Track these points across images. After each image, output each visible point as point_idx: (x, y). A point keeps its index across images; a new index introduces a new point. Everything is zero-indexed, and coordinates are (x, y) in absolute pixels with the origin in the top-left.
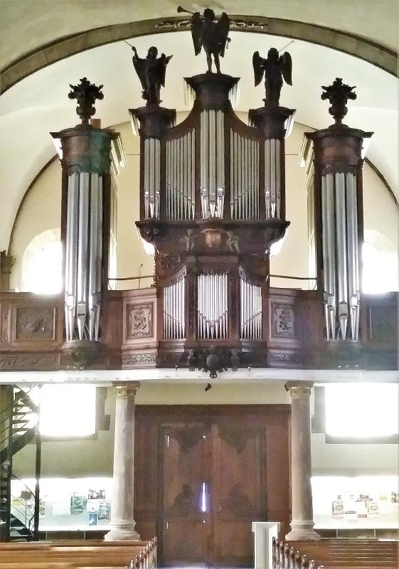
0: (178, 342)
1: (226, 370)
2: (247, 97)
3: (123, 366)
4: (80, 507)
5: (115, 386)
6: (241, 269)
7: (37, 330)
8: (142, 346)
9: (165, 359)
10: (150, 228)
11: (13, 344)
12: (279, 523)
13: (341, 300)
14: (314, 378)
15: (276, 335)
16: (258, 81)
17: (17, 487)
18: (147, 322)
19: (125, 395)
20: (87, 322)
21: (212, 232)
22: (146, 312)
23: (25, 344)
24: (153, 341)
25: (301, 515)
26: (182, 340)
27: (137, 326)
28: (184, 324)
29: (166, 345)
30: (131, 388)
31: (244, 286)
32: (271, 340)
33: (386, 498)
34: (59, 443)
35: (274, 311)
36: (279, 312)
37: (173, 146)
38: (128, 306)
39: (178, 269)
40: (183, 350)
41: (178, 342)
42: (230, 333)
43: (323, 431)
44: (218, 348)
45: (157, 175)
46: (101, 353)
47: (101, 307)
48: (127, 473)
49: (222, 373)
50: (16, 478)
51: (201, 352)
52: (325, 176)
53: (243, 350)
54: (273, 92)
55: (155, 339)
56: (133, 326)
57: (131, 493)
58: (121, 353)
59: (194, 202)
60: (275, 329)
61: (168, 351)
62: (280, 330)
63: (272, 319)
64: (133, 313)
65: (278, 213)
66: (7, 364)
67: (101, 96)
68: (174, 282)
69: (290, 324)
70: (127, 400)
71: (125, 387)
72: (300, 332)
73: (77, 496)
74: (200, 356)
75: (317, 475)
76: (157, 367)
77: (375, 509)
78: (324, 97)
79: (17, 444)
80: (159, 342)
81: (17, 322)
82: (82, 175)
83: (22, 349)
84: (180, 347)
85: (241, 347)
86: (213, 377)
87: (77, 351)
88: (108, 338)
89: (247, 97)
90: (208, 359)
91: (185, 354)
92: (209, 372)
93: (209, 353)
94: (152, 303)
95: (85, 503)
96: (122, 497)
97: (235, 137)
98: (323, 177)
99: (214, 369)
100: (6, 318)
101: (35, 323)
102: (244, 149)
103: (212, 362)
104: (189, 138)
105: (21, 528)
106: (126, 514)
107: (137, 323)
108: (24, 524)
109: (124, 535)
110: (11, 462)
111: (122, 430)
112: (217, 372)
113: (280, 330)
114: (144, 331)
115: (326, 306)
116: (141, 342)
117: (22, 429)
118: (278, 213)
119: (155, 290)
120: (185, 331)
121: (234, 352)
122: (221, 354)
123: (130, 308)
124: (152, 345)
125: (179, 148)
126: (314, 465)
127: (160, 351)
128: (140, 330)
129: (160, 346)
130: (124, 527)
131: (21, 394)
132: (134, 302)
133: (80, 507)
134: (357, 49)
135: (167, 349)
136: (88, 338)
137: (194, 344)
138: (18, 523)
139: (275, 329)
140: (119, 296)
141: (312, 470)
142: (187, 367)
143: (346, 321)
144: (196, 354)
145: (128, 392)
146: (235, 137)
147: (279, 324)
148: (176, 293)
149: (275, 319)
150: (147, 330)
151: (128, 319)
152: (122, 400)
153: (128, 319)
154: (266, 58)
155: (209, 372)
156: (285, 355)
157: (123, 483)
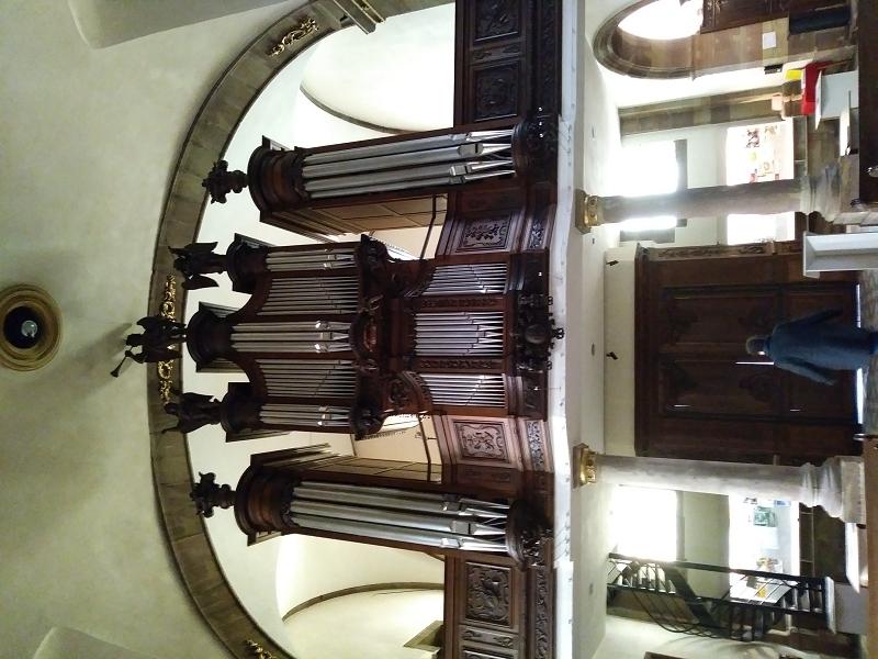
1: (551, 314)
2: (224, 294)
3: (548, 470)
4: (768, 515)
6: (410, 294)
7: (495, 593)
8: (515, 439)
9: (534, 406)
10: (364, 422)
12: (805, 234)
13: (457, 156)
14: (569, 188)
16: (213, 284)
17: (740, 590)
18: (482, 431)
21: (369, 337)
22: (469, 431)
23: (517, 618)
25: (792, 195)
26: (504, 379)
27: (489, 446)
28: (482, 377)
29: (513, 405)
30: (583, 458)
33: (755, 154)
34: (686, 545)
36: (471, 241)
37: (275, 387)
38: (464, 457)
39: (406, 383)
40: (519, 379)
44: (517, 327)
45: (303, 406)
46: (526, 505)
48: (718, 473)
49: (558, 321)
51: (522, 350)
52: (310, 193)
53: (520, 287)
54: (218, 264)
56: (490, 451)
57: (755, 469)
58: (528, 471)
59: (336, 362)
60: (496, 246)
62: (496, 239)
64: (472, 450)
66: (546, 645)
68: (426, 389)
69: (491, 225)
70: (603, 468)
71: (582, 467)
72: (502, 212)
73: (752, 518)
74: (528, 352)
76: (545, 419)
77: (768, 164)
78: (223, 200)
79: (685, 591)
82: (293, 509)
84: (515, 384)
85: (515, 291)
86: (562, 334)
89: (224, 294)
90: (532, 340)
91: (524, 374)
92: (555, 340)
93: (522, 340)
94: (455, 422)
95: (762, 509)
96: (763, 483)
97: (267, 310)
99: (550, 332)
100: (479, 636)
102: (283, 296)
103: (536, 334)
104: (267, 366)
105: (796, 592)
106: (796, 480)
107: (484, 445)
108: (789, 588)
109: (832, 484)
110: (709, 599)
111: (650, 478)
113: (496, 239)
114: (496, 436)
116: (510, 440)
119: (437, 417)
120: (487, 374)
122: (526, 320)
123: (465, 455)
124: (513, 426)
125: (279, 379)
128: (494, 440)
129: (514, 413)
130: (817, 485)
131: (625, 574)
132: (457, 450)
133: (768, 515)
134: (198, 175)
135: (518, 402)
136: (504, 519)
137: (509, 363)
138: (788, 596)
139: (496, 246)
140: (449, 466)
143: (484, 145)
144: (525, 360)
145: (590, 463)
146: (267, 310)
147: (488, 240)
150: (493, 431)
152: (602, 475)
155: (555, 340)
157: (739, 481)
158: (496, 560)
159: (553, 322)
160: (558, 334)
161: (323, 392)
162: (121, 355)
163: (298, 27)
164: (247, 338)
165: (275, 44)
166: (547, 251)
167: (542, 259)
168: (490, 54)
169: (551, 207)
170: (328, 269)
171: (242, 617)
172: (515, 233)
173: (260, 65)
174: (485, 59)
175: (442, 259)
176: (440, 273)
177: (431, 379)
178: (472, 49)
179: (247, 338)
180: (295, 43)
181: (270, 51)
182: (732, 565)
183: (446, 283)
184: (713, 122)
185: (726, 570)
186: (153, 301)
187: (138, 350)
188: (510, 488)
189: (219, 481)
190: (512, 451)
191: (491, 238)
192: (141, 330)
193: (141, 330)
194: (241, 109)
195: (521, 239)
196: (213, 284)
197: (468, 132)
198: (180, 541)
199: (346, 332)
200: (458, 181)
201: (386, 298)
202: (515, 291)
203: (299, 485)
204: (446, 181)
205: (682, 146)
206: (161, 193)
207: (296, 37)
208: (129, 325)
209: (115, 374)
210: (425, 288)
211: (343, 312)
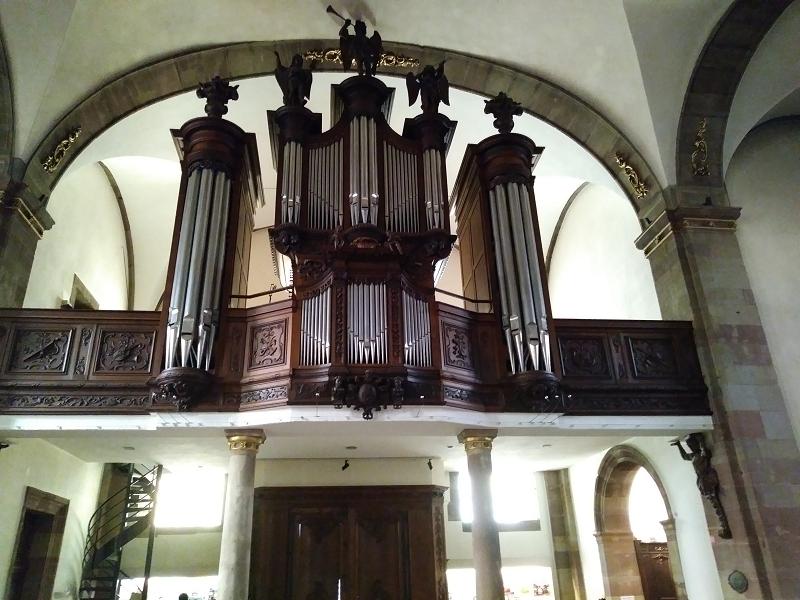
0: (321, 369)
1: (385, 408)
2: (402, 111)
5: (228, 437)
9: (302, 392)
10: (285, 238)
11: (91, 377)
13: (527, 321)
15: (449, 362)
16: (412, 101)
18: (277, 345)
19: (242, 449)
20: (195, 345)
22: (277, 333)
24: (286, 368)
27: (264, 352)
29: (303, 374)
30: (253, 438)
31: (406, 298)
32: (444, 368)
35: (445, 334)
36: (452, 335)
37: (317, 156)
38: (253, 329)
39: (321, 278)
40: (326, 379)
41: (321, 369)
42: (391, 353)
43: (459, 520)
44: (374, 376)
45: (300, 182)
47: (217, 329)
48: (239, 563)
49: (379, 414)
50: (127, 576)
51: (352, 381)
52: (494, 189)
53: (410, 379)
54: (430, 106)
55: (287, 366)
56: (259, 352)
60: (447, 356)
61: (307, 381)
62: (453, 357)
63: (445, 343)
64: (260, 336)
65: (442, 224)
67: (235, 97)
68: (316, 294)
69: (465, 352)
70: (244, 457)
71: (244, 438)
72: (477, 364)
74: (351, 387)
75: (453, 567)
76: (289, 403)
80: (294, 370)
81: (101, 349)
82: (205, 171)
83: (101, 385)
84: (322, 375)
85: (407, 374)
86: (367, 418)
87: (175, 381)
88: (224, 371)
89: (402, 111)
91: (331, 384)
93: (362, 381)
94: (286, 320)
98: (491, 193)
99: (369, 406)
100: (86, 344)
101: (126, 351)
102: (401, 166)
103: (367, 394)
104: (337, 148)
107: (264, 347)
110: (120, 559)
112: (373, 411)
113: (453, 357)
114: (273, 357)
115: (507, 331)
116: (269, 371)
117: (131, 519)
118: (442, 224)
121: (397, 381)
122: (380, 384)
123: (255, 330)
124: (282, 374)
126: (504, 553)
127: (295, 381)
129: (294, 374)
139: (447, 356)
140: (244, 315)
141: (502, 562)
142: (331, 403)
143: (537, 346)
144: (344, 384)
146: (389, 151)
147: (452, 350)
148: (321, 307)
149: (447, 344)
150: (277, 355)
151: (252, 342)
153: (252, 342)
154: (400, 133)
156: (462, 390)
158: (158, 358)
159: (379, 409)
160: (368, 414)
161: (313, 200)
162: (347, 16)
163: (640, 180)
164: (362, 131)
165: (626, 160)
166: (444, 403)
167: (435, 398)
168: (617, 351)
169: (482, 406)
170: (425, 206)
171: (103, 124)
172: (458, 375)
173: (607, 145)
174: (613, 348)
175: (435, 309)
176: (422, 306)
177: (326, 297)
178: (622, 335)
179: (362, 131)
180: (626, 178)
181: (619, 155)
182: (152, 581)
183: (415, 315)
184: (557, 554)
185: (147, 573)
186: (395, 46)
187: (351, 31)
188: (224, 371)
189: (231, 104)
190: (258, 374)
191: (454, 353)
192: (370, 34)
193: (370, 34)
194: (568, 128)
195: (453, 379)
196: (412, 101)
197: (549, 331)
198: (174, 67)
199: (369, 220)
200: (505, 323)
201: (399, 258)
202: (407, 374)
203: (227, 178)
204: (505, 312)
205: (534, 526)
206: (493, 54)
207: (631, 178)
208: (374, 23)
209: (330, 10)
210: (409, 292)
211: (387, 219)
